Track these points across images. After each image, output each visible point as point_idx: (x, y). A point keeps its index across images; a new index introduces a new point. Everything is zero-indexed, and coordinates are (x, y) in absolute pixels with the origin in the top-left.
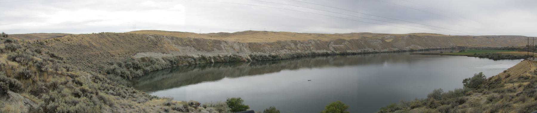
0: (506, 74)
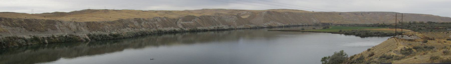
0: (370, 53)
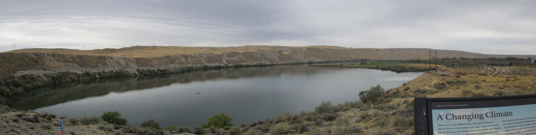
0: (405, 87)
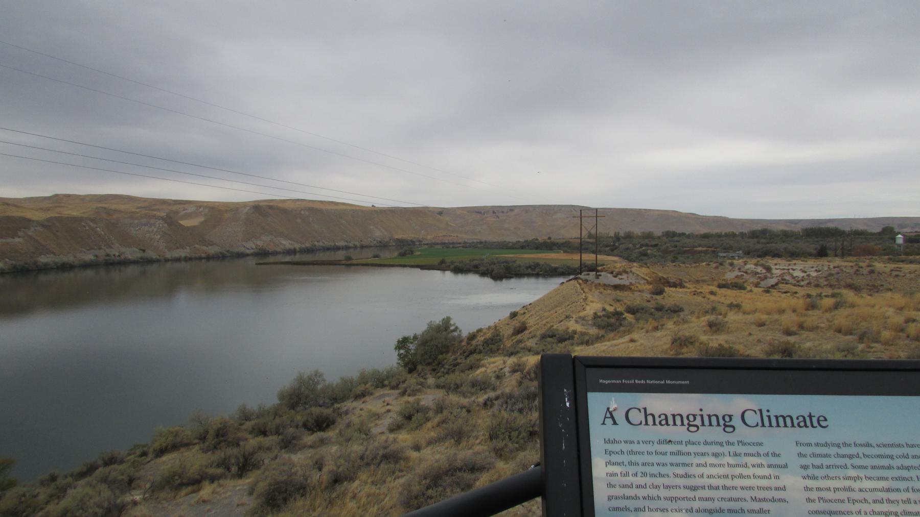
0: (516, 323)
